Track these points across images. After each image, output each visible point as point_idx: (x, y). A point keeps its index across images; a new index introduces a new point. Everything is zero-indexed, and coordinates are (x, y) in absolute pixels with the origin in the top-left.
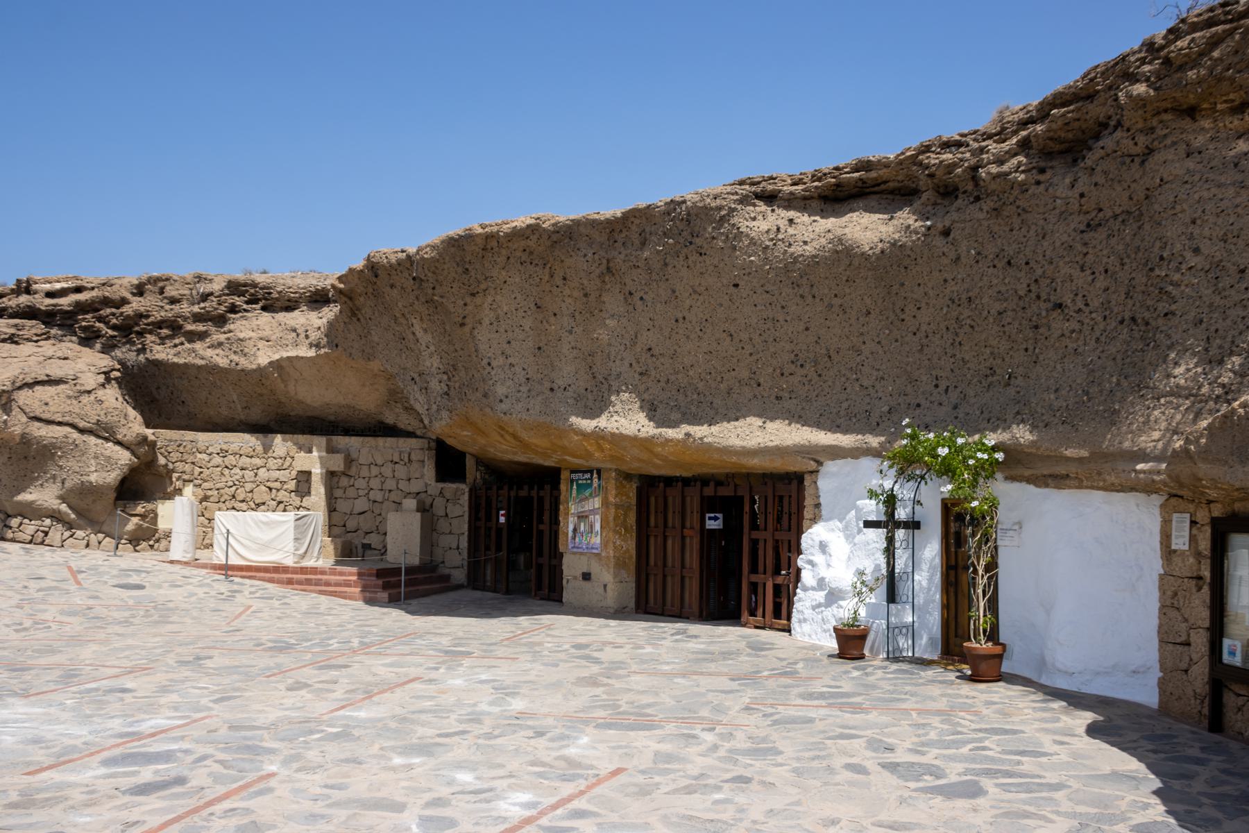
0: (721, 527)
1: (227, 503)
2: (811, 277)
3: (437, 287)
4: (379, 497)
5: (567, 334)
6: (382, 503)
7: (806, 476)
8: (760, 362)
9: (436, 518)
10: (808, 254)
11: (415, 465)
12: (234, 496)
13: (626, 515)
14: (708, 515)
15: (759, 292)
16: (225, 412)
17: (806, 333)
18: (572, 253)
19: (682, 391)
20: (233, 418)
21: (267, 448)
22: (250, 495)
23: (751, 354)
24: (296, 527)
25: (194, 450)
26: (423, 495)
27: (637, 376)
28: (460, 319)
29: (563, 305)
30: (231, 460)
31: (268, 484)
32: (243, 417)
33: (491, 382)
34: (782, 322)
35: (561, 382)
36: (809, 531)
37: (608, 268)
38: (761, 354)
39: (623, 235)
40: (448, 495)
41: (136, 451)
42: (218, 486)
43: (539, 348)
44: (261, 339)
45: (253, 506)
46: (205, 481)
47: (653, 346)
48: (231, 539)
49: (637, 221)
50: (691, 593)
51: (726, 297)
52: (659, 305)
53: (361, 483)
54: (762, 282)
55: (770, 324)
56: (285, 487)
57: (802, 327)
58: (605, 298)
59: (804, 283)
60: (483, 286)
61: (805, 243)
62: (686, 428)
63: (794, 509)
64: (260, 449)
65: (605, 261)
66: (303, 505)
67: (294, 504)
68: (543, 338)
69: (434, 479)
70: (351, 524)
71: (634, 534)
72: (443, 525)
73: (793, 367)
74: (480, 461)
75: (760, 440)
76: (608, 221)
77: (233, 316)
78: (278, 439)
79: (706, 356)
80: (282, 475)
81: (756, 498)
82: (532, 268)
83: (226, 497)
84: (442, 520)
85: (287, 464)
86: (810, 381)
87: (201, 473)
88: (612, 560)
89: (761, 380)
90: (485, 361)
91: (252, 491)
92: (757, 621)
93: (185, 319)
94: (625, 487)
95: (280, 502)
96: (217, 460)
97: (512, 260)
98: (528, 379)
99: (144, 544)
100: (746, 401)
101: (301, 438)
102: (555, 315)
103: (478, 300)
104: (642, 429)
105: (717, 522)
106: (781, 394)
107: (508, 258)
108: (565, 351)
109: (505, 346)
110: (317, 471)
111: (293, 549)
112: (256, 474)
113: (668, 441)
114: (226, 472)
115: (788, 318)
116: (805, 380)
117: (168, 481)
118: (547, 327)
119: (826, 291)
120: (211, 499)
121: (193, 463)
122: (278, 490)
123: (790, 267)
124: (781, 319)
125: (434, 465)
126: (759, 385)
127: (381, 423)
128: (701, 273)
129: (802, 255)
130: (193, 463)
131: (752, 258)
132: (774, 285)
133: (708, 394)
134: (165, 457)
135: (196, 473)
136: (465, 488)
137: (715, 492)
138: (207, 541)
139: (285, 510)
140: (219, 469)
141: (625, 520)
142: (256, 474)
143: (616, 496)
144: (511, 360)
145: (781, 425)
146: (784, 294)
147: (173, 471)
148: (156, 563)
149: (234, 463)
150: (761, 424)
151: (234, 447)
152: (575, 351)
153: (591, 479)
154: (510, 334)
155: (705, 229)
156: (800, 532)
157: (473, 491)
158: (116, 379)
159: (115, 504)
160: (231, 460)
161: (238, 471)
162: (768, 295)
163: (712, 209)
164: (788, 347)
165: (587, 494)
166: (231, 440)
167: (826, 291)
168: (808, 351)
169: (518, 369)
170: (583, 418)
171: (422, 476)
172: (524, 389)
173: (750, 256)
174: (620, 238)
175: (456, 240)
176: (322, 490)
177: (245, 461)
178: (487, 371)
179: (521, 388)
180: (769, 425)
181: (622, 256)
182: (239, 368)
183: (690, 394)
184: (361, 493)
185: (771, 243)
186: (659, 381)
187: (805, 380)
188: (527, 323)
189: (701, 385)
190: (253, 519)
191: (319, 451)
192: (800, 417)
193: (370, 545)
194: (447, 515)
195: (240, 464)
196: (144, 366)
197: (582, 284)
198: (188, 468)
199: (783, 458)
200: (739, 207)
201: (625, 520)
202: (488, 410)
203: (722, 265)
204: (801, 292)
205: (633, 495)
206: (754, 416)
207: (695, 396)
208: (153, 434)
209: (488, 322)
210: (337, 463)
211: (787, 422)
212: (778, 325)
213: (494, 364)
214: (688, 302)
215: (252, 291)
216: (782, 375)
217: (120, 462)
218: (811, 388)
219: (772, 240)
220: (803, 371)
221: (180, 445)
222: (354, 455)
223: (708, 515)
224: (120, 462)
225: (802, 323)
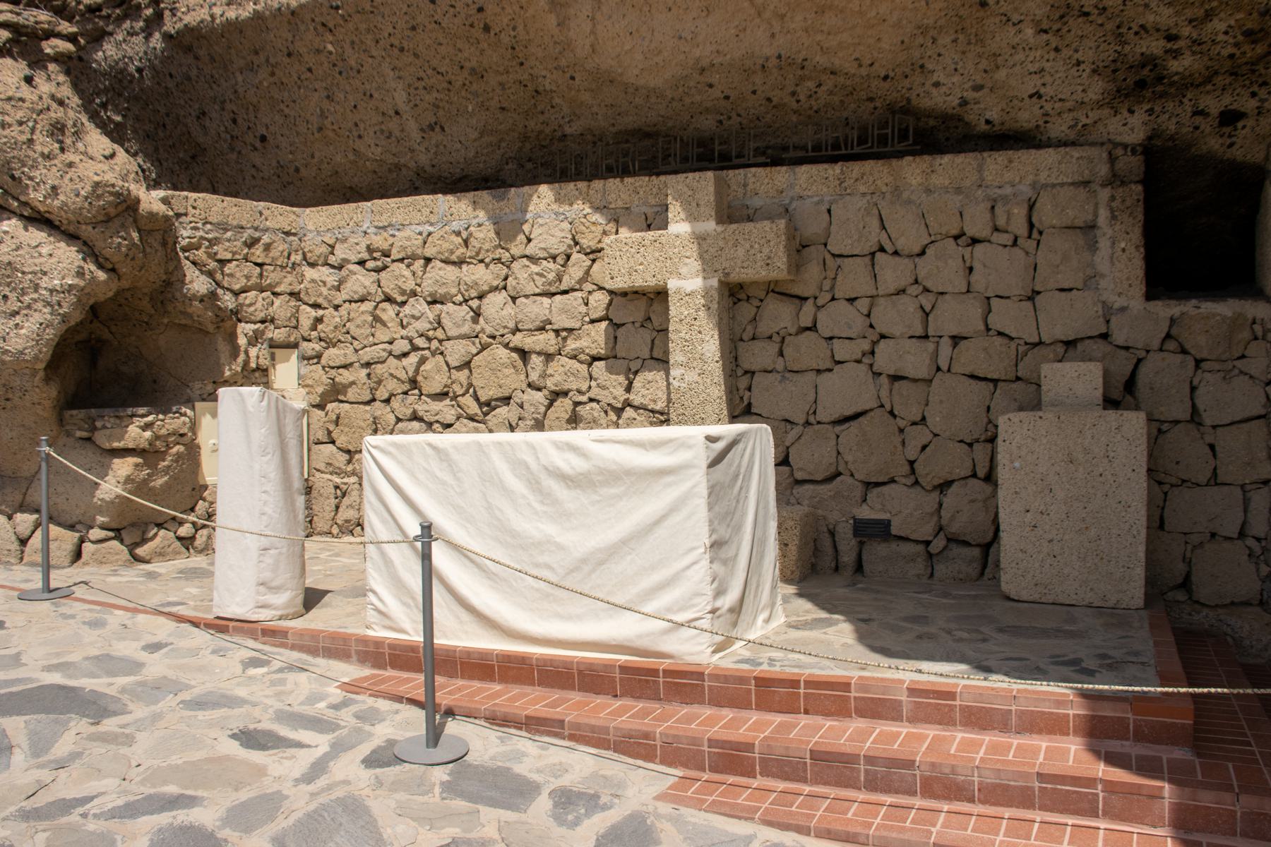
1: (395, 403)
4: (915, 360)
12: (414, 383)
16: (373, 148)
20: (398, 167)
21: (508, 229)
22: (462, 376)
25: (296, 258)
30: (399, 277)
31: (517, 340)
32: (424, 159)
41: (99, 245)
42: (367, 355)
45: (474, 408)
46: (331, 344)
48: (439, 555)
56: (572, 345)
64: (485, 235)
66: (636, 399)
67: (605, 397)
69: (1139, 289)
78: (543, 197)
80: (562, 310)
83: (392, 385)
85: (574, 273)
87: (319, 320)
91: (467, 365)
95: (557, 395)
96: (361, 281)
99: (163, 537)
101: (617, 190)
112: (477, 314)
114: (388, 312)
117: (223, 346)
120: (351, 394)
121: (294, 295)
122: (549, 357)
125: (1137, 235)
127: (907, 110)
130: (294, 295)
134: (210, 274)
135: (306, 323)
138: (345, 514)
139: (574, 421)
140: (368, 306)
142: (477, 314)
147: (237, 315)
148: (163, 629)
149: (410, 285)
151: (406, 239)
158: (58, 58)
159: (61, 421)
160: (399, 277)
161: (423, 307)
166: (398, 218)
171: (1091, 280)
176: (711, 346)
177: (441, 277)
190: (520, 467)
191: (692, 217)
193: (886, 524)
195: (428, 287)
196: (166, 60)
198: (281, 307)
208: (165, 201)
217: (45, 282)
221: (252, 243)
224: (45, 282)
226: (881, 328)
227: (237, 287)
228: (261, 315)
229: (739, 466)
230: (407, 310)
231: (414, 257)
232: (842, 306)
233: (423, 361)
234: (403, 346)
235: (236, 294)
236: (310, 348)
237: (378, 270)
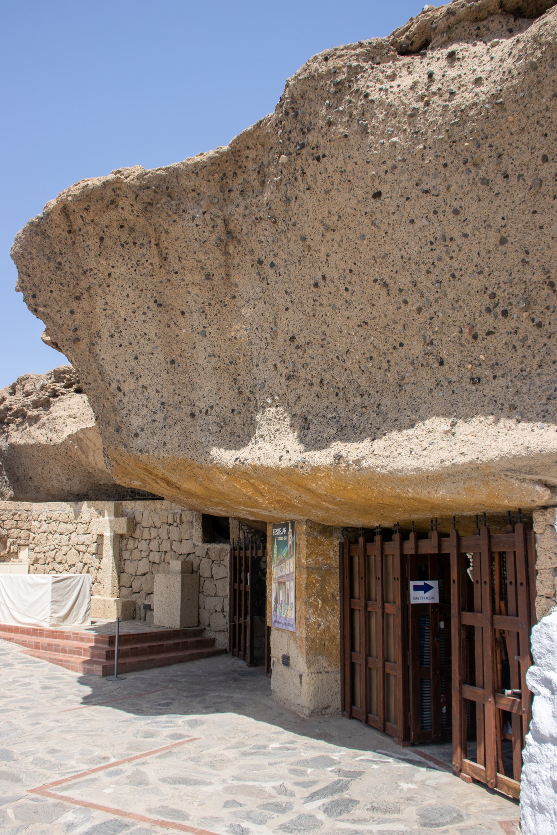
0: (437, 601)
2: (496, 141)
3: (38, 294)
5: (200, 337)
6: (159, 564)
7: (535, 515)
8: (436, 322)
9: (202, 580)
10: (483, 97)
11: (185, 526)
13: (323, 582)
14: (412, 584)
15: (412, 196)
17: (502, 248)
18: (176, 217)
19: (341, 394)
21: (77, 514)
23: (419, 310)
24: (54, 590)
26: (192, 556)
27: (283, 380)
28: (70, 334)
29: (189, 298)
31: (77, 547)
33: (124, 412)
34: (459, 240)
35: (202, 405)
36: (545, 619)
37: (229, 233)
38: (435, 307)
39: (240, 181)
40: (213, 555)
43: (173, 362)
44: (70, 416)
46: (37, 545)
47: (296, 332)
49: (252, 154)
50: (396, 700)
51: (366, 220)
52: (293, 268)
53: (143, 545)
54: (416, 176)
55: (440, 249)
57: (493, 238)
58: (236, 278)
59: (485, 156)
60: (84, 284)
61: (478, 81)
62: (338, 447)
63: (521, 578)
64: (72, 515)
65: (220, 222)
68: (174, 347)
69: (201, 540)
70: (136, 586)
71: (337, 608)
72: (208, 587)
73: (490, 319)
74: (241, 522)
75: (443, 455)
76: (213, 161)
77: (55, 399)
79: (361, 332)
81: (470, 557)
82: (136, 249)
84: (208, 581)
86: (525, 339)
88: (304, 643)
89: (444, 354)
90: (114, 386)
92: (475, 770)
93: (28, 406)
94: (322, 544)
95: (86, 564)
96: (45, 526)
97: (107, 242)
98: (163, 404)
100: (425, 394)
102: (183, 313)
103: (85, 303)
104: (286, 457)
105: (429, 594)
106: (478, 372)
107: (102, 239)
108: (202, 361)
109: (134, 363)
110: (108, 534)
111: (50, 612)
113: (317, 469)
115: (468, 230)
116: (515, 340)
118: (177, 332)
119: (526, 157)
121: (29, 530)
122: (84, 553)
123: (457, 133)
124: (456, 234)
126: (441, 363)
128: (327, 192)
129: (475, 104)
130: (29, 530)
131: (395, 139)
132: (435, 176)
133: (373, 392)
135: (31, 538)
136: (227, 547)
137: (417, 547)
140: (46, 534)
141: (323, 588)
143: (308, 556)
144: (143, 381)
145: (480, 427)
146: (454, 188)
150: (447, 428)
151: (55, 515)
152: (213, 359)
153: (287, 535)
154: (135, 346)
155: (316, 113)
156: (532, 620)
157: (233, 549)
162: (429, 198)
163: (321, 77)
164: (477, 283)
165: (284, 554)
166: (54, 508)
167: (526, 157)
168: (511, 283)
169: (151, 392)
170: (226, 449)
171: (191, 537)
172: (159, 417)
173: (391, 136)
174: (236, 184)
175: (38, 225)
177: (63, 525)
178: (118, 398)
179: (157, 417)
180: (462, 428)
181: (241, 210)
182: (52, 443)
183: (352, 398)
184: (144, 554)
185: (421, 104)
186: (312, 384)
187: (515, 340)
188: (152, 329)
189: (363, 380)
191: (109, 515)
192: (513, 407)
194: (212, 577)
197: (199, 261)
199: (487, 484)
200: (366, 66)
201: (323, 588)
202: (121, 448)
203: (349, 168)
204: (482, 174)
205: (334, 554)
206: (438, 415)
207: (358, 400)
209: (107, 334)
210: (122, 526)
211: (491, 418)
212: (453, 246)
213: (125, 388)
214: (323, 249)
215: (68, 376)
216: (475, 337)
218: (529, 353)
219: (422, 97)
220: (510, 324)
221: (15, 514)
222: (138, 519)
223: (412, 584)
225: (492, 233)
226: (151, 549)
227: (8, 528)
228: (16, 536)
229: (70, 584)
230: (54, 536)
231: (57, 520)
232: (143, 541)
233: (57, 552)
234: (52, 547)
235: (8, 530)
236: (32, 546)
237: (49, 523)
